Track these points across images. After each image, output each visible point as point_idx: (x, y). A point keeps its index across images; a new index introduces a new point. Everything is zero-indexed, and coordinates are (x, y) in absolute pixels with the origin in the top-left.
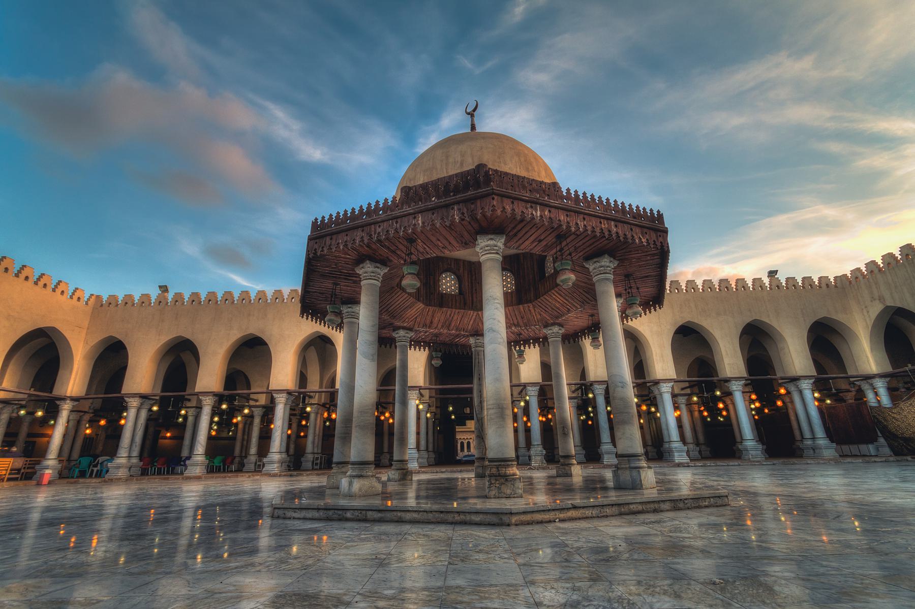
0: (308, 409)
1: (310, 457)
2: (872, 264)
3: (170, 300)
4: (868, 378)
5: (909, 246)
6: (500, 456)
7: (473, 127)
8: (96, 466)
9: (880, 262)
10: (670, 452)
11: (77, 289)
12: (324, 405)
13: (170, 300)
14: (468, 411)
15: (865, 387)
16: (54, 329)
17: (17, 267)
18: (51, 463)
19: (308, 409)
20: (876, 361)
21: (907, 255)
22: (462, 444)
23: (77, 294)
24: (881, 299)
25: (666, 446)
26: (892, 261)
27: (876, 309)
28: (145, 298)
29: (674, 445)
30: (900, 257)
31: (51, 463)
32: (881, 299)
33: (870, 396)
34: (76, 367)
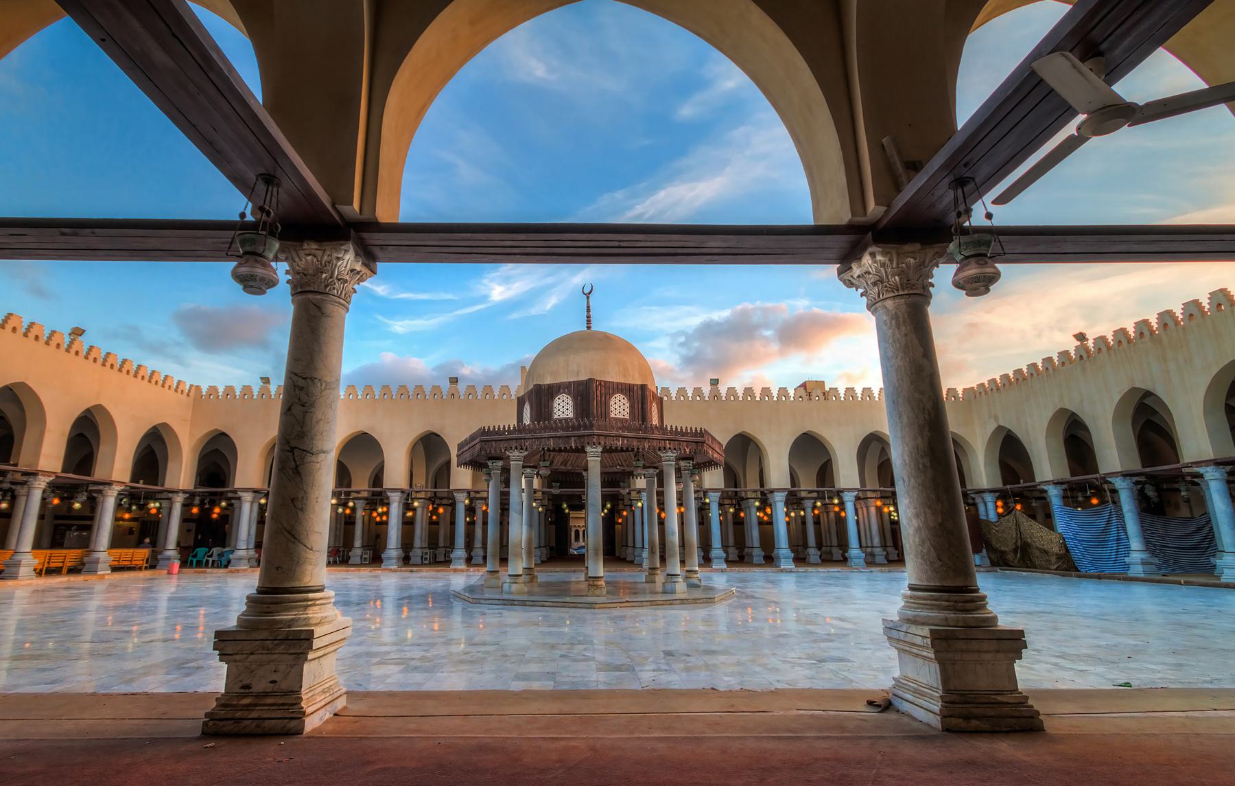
0: (416, 504)
1: (419, 552)
2: (1018, 372)
3: (273, 393)
4: (980, 492)
5: (1224, 292)
6: (908, 657)
7: (589, 328)
8: (211, 556)
9: (1205, 303)
10: (751, 555)
11: (92, 347)
12: (429, 499)
13: (273, 393)
14: (619, 407)
15: (978, 500)
16: (23, 385)
17: (47, 334)
18: (171, 549)
19: (416, 504)
20: (987, 476)
21: (1219, 305)
22: (577, 532)
23: (181, 387)
24: (996, 418)
25: (776, 551)
26: (1195, 311)
27: (992, 426)
28: (247, 389)
29: (782, 552)
30: (1181, 317)
31: (171, 549)
32: (996, 418)
33: (981, 508)
34: (184, 460)
